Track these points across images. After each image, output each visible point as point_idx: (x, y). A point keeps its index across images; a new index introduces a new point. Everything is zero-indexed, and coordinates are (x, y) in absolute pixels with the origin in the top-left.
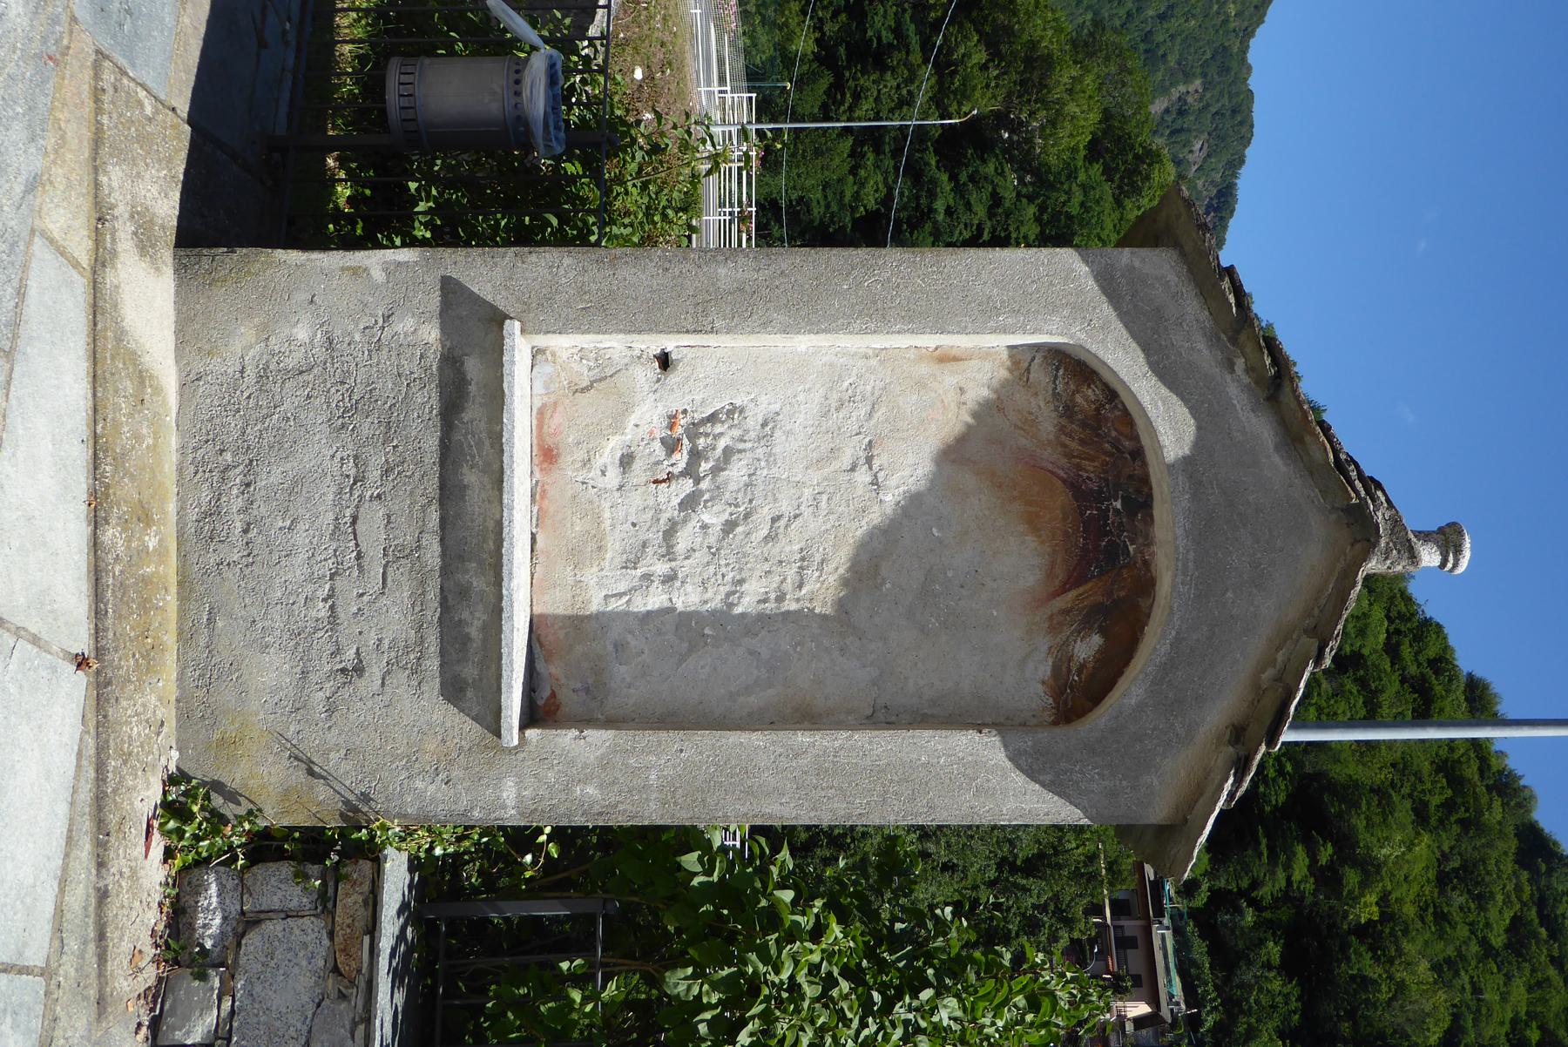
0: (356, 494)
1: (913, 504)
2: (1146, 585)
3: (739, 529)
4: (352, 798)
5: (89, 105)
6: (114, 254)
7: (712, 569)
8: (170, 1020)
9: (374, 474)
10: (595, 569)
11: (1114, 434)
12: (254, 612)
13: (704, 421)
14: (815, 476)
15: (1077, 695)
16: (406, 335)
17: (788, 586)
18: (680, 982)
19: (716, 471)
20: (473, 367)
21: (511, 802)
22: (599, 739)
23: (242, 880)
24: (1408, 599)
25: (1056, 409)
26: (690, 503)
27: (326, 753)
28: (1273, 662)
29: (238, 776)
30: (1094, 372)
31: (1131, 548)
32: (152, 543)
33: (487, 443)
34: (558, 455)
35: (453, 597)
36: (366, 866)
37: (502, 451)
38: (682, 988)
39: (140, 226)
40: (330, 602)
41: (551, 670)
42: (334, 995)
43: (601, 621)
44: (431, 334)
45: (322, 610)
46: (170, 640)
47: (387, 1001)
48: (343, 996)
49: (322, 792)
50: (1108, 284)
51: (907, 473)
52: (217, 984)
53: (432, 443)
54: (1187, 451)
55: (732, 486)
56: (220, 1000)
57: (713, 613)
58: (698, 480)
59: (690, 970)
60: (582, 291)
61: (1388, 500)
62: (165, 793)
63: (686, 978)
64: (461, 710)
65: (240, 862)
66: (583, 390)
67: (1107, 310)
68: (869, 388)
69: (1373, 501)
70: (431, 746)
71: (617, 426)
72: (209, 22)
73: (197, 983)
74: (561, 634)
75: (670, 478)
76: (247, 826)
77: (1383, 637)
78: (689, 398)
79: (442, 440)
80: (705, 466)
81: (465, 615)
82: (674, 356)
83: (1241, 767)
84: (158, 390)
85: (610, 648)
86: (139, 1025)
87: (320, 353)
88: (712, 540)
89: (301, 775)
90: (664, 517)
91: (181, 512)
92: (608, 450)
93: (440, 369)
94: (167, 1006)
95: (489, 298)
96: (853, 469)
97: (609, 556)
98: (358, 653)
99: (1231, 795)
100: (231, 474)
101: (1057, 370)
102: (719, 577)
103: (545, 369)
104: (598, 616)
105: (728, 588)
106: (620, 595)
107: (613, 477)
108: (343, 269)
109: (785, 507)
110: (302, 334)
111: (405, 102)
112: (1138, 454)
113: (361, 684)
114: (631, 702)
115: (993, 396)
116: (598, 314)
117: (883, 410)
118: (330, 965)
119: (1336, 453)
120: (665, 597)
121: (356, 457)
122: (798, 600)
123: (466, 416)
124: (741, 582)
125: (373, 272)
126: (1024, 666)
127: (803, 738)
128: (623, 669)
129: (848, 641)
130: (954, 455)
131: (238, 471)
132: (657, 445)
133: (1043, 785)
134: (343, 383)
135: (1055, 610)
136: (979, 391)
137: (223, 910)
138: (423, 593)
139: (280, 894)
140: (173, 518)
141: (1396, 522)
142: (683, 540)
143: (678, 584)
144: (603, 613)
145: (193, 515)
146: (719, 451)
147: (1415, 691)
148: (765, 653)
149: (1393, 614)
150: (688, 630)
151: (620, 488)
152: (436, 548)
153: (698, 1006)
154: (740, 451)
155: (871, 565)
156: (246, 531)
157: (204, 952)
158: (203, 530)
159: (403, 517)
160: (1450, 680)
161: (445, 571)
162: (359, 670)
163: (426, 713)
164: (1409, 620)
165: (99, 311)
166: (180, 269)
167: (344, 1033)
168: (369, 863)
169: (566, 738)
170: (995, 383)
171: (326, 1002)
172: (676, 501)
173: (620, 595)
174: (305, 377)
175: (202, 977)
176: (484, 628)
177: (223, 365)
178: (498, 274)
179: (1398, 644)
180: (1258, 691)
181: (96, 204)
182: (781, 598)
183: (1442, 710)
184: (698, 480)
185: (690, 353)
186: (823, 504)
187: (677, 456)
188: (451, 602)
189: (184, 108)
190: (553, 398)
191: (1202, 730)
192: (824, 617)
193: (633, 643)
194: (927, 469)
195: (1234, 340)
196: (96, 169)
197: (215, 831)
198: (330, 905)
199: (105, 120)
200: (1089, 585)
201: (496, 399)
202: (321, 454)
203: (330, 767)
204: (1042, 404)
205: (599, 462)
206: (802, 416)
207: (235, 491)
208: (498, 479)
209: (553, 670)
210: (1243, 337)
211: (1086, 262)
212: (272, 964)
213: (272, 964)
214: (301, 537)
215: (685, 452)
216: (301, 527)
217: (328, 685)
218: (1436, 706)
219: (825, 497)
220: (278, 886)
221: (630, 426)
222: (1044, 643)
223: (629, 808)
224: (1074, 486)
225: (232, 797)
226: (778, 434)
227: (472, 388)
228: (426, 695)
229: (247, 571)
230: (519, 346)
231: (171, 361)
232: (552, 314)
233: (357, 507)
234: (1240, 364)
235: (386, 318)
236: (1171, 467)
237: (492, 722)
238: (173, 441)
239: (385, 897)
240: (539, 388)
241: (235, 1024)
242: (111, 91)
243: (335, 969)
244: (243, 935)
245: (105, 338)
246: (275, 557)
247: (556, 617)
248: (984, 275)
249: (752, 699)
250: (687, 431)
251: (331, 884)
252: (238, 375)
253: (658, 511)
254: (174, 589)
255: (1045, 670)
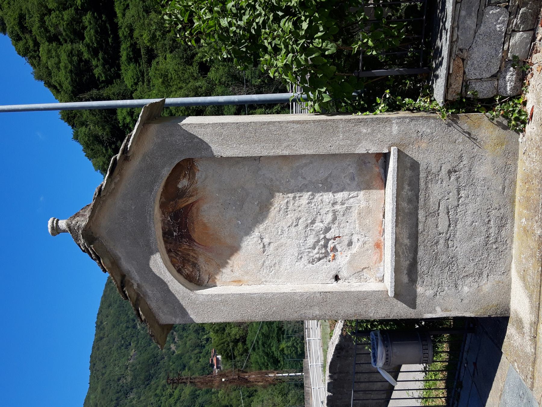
0: (448, 235)
1: (248, 232)
2: (163, 206)
3: (309, 221)
4: (454, 125)
5: (536, 375)
6: (531, 325)
7: (319, 207)
8: (528, 41)
9: (442, 241)
10: (362, 206)
11: (178, 258)
12: (488, 192)
13: (323, 258)
14: (283, 241)
15: (185, 167)
16: (429, 289)
17: (292, 202)
18: (331, 48)
19: (318, 241)
20: (405, 279)
21: (395, 125)
22: (361, 150)
23: (497, 92)
24: (32, 64)
25: (199, 266)
26: (327, 229)
27: (463, 141)
28: (116, 184)
29: (497, 132)
30: (186, 279)
31: (169, 218)
32: (524, 220)
33: (400, 253)
34: (374, 246)
35: (414, 200)
36: (450, 98)
37: (395, 252)
38: (329, 46)
39: (521, 329)
40: (459, 196)
41: (377, 170)
42: (464, 51)
43: (359, 188)
44: (420, 290)
45: (463, 194)
46: (519, 183)
47: (444, 43)
48: (461, 50)
49: (465, 127)
50: (183, 312)
51: (250, 243)
52: (509, 54)
53: (420, 253)
54: (152, 257)
55: (312, 236)
56: (508, 48)
57: (319, 192)
58: (325, 237)
59: (327, 53)
60: (366, 305)
61: (80, 247)
62: (525, 127)
63: (328, 50)
64: (412, 159)
65: (498, 98)
66: (366, 268)
67: (183, 303)
68: (265, 271)
69: (85, 246)
70: (424, 145)
71: (354, 256)
72: (493, 380)
73: (517, 55)
74: (374, 183)
75: (335, 238)
76: (494, 113)
77: (41, 49)
78: (328, 266)
79: (417, 254)
80: (322, 242)
81: (410, 193)
82: (334, 280)
83: (125, 150)
84: (518, 272)
85: (356, 178)
86: (540, 41)
87: (459, 282)
88: (319, 217)
89: (473, 133)
90: (336, 225)
91: (512, 226)
92: (357, 247)
93: (417, 278)
94: (529, 46)
95: (399, 302)
96: (270, 243)
97: (357, 211)
98: (450, 178)
99: (128, 140)
100: (494, 241)
101: (199, 279)
102: (316, 205)
103: (379, 275)
104: (360, 190)
105: (313, 201)
106: (352, 197)
107: (355, 238)
108: (451, 311)
109: (293, 229)
110: (466, 289)
111: (426, 351)
112: (169, 251)
113: (449, 167)
114: (349, 159)
115: (221, 270)
116: (361, 297)
117: (260, 264)
118: (465, 62)
119: (100, 262)
120: (336, 197)
121: (448, 247)
122: (288, 197)
123: (408, 262)
124: (309, 203)
125: (440, 310)
126: (206, 181)
127: (286, 153)
128: (351, 171)
129: (270, 183)
130: (234, 249)
131: (491, 242)
132: (339, 249)
133: (197, 137)
134: (452, 273)
135: (195, 196)
136: (226, 271)
137: (505, 81)
138: (425, 200)
139: (483, 87)
140: (516, 225)
141: (76, 239)
142: (330, 217)
143: (332, 202)
144: (359, 190)
145: (508, 226)
146: (317, 248)
147: (26, 27)
148: (300, 178)
149: (37, 58)
150: (328, 185)
151: (352, 235)
152: (420, 217)
153: (323, 38)
154: (310, 248)
155: (263, 210)
156: (489, 221)
157: (513, 66)
158: (504, 221)
159: (431, 227)
160: (12, 32)
161: (416, 208)
162: (450, 172)
163: (425, 157)
164: (31, 56)
165: (537, 308)
166: (508, 310)
167: (461, 38)
168: (449, 99)
169: (373, 150)
170: (220, 274)
171: (467, 48)
172: (332, 230)
173: (352, 197)
174: (465, 274)
175: (514, 57)
176: (403, 188)
177: (494, 278)
178: (396, 310)
179: (34, 46)
180: (121, 174)
181: (536, 343)
182: (294, 198)
183: (14, 20)
184: (325, 237)
185: (328, 281)
186: (280, 231)
187: (332, 246)
188: (415, 197)
189: (503, 357)
190: (376, 265)
191: (140, 159)
192: (279, 192)
193: (348, 180)
194: (243, 244)
195: (138, 295)
196: (535, 354)
197: (507, 112)
198: (464, 84)
199: (531, 369)
200: (183, 206)
201: (397, 270)
202: (461, 248)
203: (462, 136)
204: (204, 267)
205: (360, 243)
206: (288, 261)
207: (493, 235)
208: (397, 242)
209: (377, 170)
210: (134, 297)
211: (191, 319)
212: (487, 62)
213: (487, 62)
214: (469, 219)
215: (329, 247)
216: (469, 223)
217: (462, 166)
218: (17, 21)
219: (279, 233)
220: (483, 90)
221: (349, 256)
222: (199, 185)
223: (350, 125)
224: (191, 240)
225: (499, 124)
226: (297, 255)
227: (405, 272)
228: (425, 164)
229: (490, 207)
230: (388, 285)
231: (513, 280)
232: (378, 297)
233: (448, 230)
234: (135, 287)
235: (436, 295)
236: (157, 251)
237: (400, 153)
238: (514, 252)
239: (443, 88)
240: (381, 269)
241: (503, 40)
242: (528, 377)
243: (463, 60)
244: (498, 72)
245: (536, 299)
246: (479, 212)
247: (376, 189)
248: (226, 313)
249: (304, 162)
250: (328, 254)
251: (463, 91)
252: (489, 274)
253: (339, 227)
254: (517, 200)
255: (198, 175)
